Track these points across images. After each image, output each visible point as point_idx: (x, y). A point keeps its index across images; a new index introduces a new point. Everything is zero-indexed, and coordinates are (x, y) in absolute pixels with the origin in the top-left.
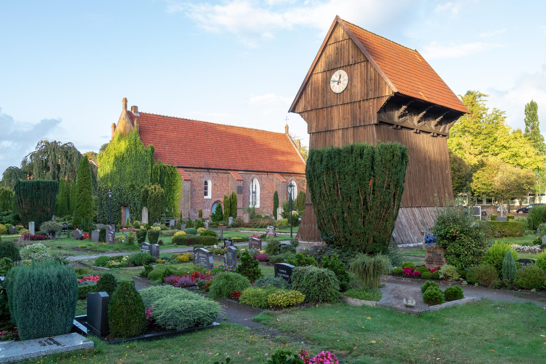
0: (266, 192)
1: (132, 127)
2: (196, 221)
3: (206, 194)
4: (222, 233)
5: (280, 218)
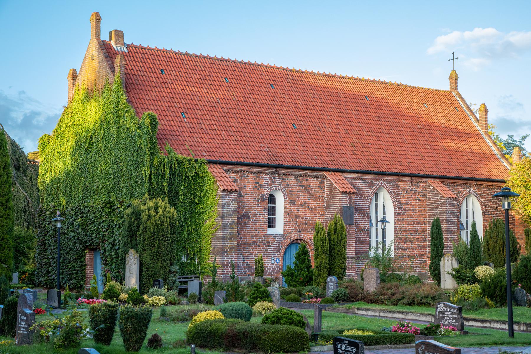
1: (111, 76)
2: (250, 284)
3: (271, 223)
4: (320, 317)
5: (448, 283)
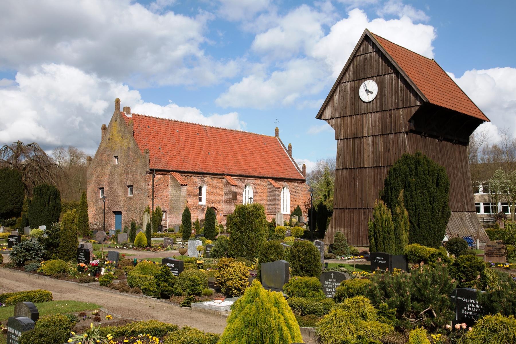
0: (260, 198)
3: (200, 200)
